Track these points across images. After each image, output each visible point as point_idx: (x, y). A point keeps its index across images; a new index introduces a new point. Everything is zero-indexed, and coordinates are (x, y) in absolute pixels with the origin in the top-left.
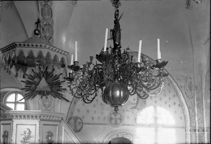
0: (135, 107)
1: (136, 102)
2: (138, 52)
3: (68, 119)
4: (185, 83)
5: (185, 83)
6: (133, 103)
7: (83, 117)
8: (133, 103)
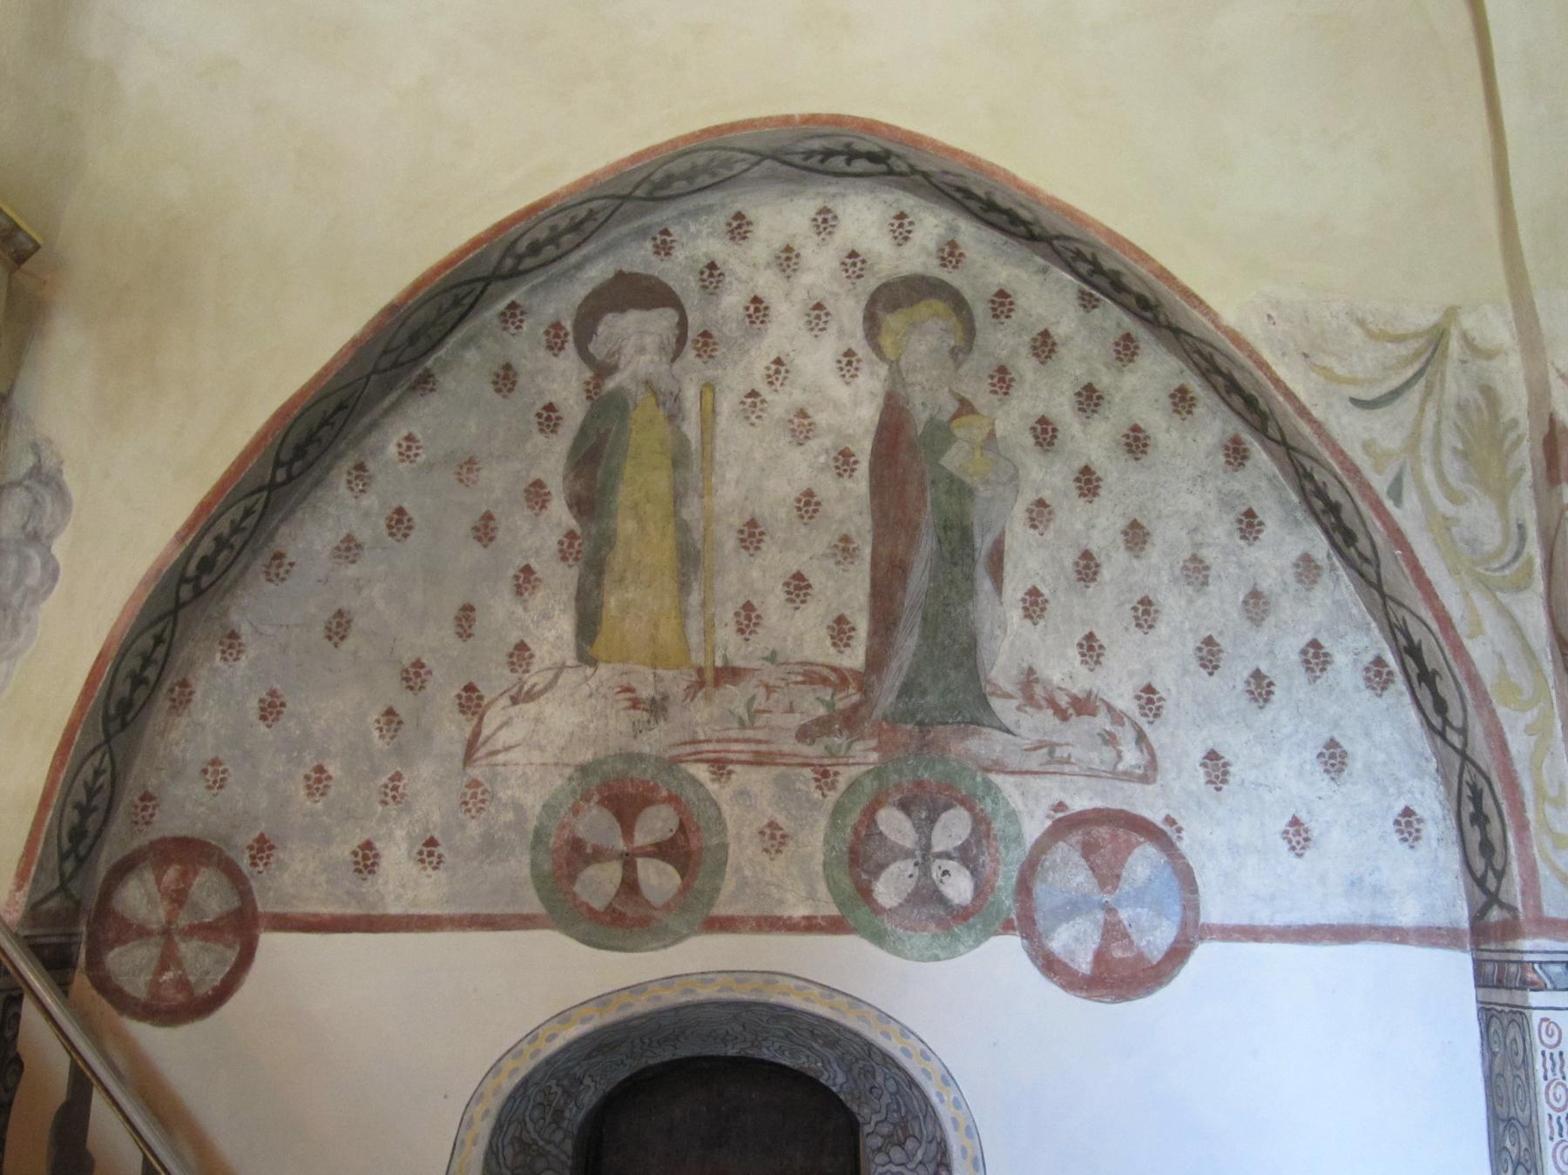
0: (855, 708)
1: (855, 658)
2: (1481, 991)
3: (1275, 392)
4: (1422, 410)
5: (1422, 410)
6: (833, 677)
7: (263, 847)
8: (833, 677)
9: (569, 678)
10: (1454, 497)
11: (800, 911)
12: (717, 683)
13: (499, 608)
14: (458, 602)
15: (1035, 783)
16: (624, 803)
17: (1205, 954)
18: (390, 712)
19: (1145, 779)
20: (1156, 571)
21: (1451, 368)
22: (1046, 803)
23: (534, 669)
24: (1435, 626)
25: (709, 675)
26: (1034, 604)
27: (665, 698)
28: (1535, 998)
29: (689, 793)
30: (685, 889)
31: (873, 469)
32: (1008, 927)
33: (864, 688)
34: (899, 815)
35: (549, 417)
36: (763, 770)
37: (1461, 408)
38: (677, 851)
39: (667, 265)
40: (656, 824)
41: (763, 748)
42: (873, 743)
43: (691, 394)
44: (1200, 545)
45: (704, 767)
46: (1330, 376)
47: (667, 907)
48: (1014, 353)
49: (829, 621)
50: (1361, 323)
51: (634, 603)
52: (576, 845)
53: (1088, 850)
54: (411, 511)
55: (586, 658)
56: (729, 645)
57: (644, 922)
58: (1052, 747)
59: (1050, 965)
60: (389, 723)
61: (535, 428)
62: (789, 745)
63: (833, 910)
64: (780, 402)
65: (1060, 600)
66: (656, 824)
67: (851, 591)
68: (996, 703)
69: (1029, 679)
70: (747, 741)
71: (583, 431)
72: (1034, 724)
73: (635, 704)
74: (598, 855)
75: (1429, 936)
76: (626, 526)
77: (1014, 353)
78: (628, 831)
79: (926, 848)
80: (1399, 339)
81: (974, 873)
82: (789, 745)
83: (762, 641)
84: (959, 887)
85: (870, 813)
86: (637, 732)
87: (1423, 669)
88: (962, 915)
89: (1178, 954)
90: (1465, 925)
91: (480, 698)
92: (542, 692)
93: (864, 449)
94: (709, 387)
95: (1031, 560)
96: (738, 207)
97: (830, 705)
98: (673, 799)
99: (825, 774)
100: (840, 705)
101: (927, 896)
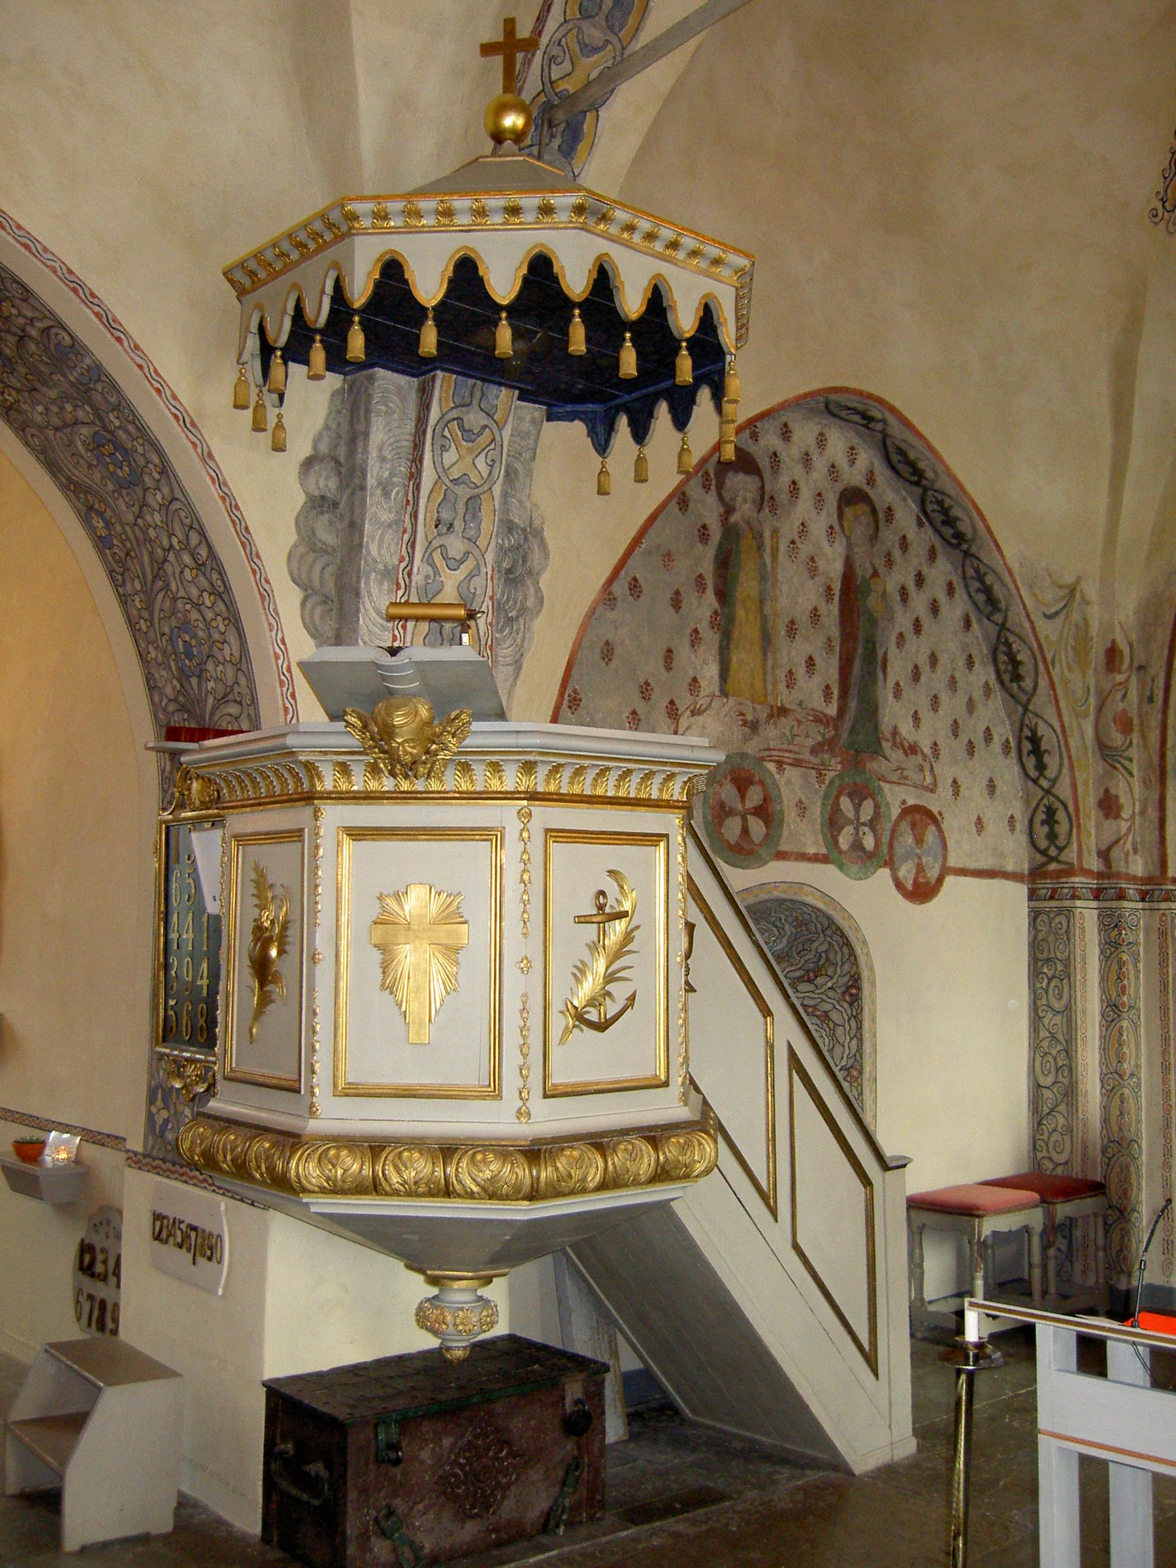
0: (833, 738)
1: (832, 710)
9: (716, 704)
10: (1069, 667)
11: (812, 850)
12: (778, 716)
13: (683, 652)
14: (665, 647)
15: (896, 788)
16: (742, 783)
17: (950, 880)
18: (634, 713)
19: (932, 791)
20: (934, 681)
21: (1076, 605)
22: (900, 799)
23: (701, 695)
24: (1058, 730)
25: (775, 711)
26: (898, 693)
27: (757, 722)
28: (1078, 903)
29: (768, 780)
30: (767, 835)
31: (840, 596)
32: (886, 864)
33: (836, 728)
34: (848, 800)
35: (704, 533)
36: (798, 769)
37: (1076, 626)
38: (761, 811)
39: (755, 447)
40: (755, 796)
41: (797, 756)
42: (839, 759)
43: (767, 534)
44: (954, 669)
45: (773, 764)
46: (1038, 601)
47: (760, 845)
48: (893, 546)
49: (823, 687)
50: (1050, 575)
51: (744, 658)
52: (722, 805)
53: (913, 825)
54: (641, 581)
55: (724, 693)
56: (785, 697)
57: (751, 853)
58: (903, 769)
59: (899, 885)
60: (634, 719)
61: (697, 539)
62: (806, 756)
63: (824, 851)
64: (805, 549)
65: (907, 691)
66: (755, 796)
67: (829, 668)
68: (884, 744)
69: (895, 732)
70: (791, 752)
71: (720, 545)
72: (896, 756)
73: (745, 723)
74: (731, 812)
75: (1015, 877)
76: (740, 613)
77: (893, 546)
78: (743, 796)
79: (858, 819)
80: (1061, 587)
81: (875, 835)
82: (806, 756)
83: (796, 695)
84: (869, 842)
85: (837, 798)
86: (746, 740)
87: (1031, 748)
88: (870, 856)
89: (940, 881)
90: (1026, 872)
91: (677, 709)
92: (705, 711)
93: (837, 587)
94: (775, 532)
95: (898, 669)
96: (785, 419)
97: (823, 735)
98: (761, 783)
99: (821, 774)
100: (827, 736)
101: (857, 845)
